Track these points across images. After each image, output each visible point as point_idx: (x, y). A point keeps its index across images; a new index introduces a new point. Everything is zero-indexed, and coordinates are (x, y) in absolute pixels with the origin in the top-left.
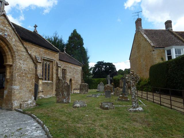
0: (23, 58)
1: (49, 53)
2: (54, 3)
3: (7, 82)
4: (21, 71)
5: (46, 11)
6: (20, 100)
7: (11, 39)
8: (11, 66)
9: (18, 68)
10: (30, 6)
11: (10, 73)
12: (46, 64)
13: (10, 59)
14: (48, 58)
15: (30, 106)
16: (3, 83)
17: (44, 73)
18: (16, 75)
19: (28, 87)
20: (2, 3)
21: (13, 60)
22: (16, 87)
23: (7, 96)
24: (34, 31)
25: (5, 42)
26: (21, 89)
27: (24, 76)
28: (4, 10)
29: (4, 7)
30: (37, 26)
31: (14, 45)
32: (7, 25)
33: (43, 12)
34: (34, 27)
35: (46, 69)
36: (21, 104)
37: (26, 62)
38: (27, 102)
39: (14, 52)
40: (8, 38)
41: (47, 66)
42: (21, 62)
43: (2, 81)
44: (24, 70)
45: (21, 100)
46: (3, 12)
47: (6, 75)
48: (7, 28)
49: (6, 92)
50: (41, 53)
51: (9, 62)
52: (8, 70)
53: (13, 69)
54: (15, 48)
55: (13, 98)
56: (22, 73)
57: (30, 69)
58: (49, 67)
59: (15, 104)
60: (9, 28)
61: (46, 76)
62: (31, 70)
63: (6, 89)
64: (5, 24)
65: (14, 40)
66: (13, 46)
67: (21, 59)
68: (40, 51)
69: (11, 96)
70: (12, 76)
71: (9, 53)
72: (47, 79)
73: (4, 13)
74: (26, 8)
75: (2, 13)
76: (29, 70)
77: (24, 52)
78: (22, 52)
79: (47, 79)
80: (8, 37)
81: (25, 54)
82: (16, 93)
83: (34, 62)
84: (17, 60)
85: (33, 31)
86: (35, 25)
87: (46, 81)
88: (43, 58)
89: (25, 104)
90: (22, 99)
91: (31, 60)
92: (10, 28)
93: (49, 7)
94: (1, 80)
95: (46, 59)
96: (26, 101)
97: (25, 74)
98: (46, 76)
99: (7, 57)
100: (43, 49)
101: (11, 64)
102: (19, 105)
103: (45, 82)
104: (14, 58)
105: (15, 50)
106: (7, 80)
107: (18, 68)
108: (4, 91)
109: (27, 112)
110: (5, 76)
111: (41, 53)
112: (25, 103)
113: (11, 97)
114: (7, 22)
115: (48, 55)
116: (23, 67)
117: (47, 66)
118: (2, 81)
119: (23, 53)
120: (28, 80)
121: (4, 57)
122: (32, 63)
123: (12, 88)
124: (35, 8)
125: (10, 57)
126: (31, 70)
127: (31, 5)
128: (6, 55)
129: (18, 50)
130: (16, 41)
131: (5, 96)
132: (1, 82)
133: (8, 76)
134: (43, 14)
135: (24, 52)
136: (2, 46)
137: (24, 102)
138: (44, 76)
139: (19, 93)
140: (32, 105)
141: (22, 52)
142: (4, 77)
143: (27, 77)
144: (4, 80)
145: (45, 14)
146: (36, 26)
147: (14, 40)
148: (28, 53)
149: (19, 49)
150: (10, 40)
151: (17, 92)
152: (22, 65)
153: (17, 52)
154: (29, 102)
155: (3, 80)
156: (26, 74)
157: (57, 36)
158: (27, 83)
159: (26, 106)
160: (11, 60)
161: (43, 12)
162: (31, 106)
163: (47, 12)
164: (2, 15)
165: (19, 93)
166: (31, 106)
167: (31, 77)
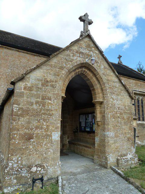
0: (116, 91)
1: (141, 84)
2: (134, 36)
3: (98, 126)
4: (115, 110)
5: (125, 47)
6: (117, 153)
7: (99, 66)
8: (101, 103)
9: (110, 105)
10: (110, 46)
11: (101, 113)
12: (138, 99)
13: (99, 94)
14: (140, 92)
15: (130, 162)
16: (92, 126)
17: (137, 111)
18: (109, 116)
19: (125, 133)
20: (86, 21)
21: (103, 95)
22: (110, 134)
23: (99, 145)
24: (119, 63)
25: (92, 72)
26: (116, 136)
27: (119, 117)
28: (89, 29)
29: (87, 27)
30: (121, 57)
31: (103, 74)
32: (93, 49)
33: (123, 48)
34: (118, 58)
35: (138, 106)
36: (118, 160)
37: (119, 97)
38: (126, 157)
39: (104, 84)
40: (95, 66)
41: (140, 102)
42: (114, 97)
43: (91, 123)
44: (119, 108)
45: (117, 153)
46: (87, 32)
47: (96, 116)
48: (93, 52)
49: (97, 140)
50: (132, 85)
51: (99, 98)
52: (98, 109)
53: (104, 108)
54: (104, 78)
55: (108, 150)
56: (116, 113)
57: (125, 106)
58: (142, 103)
59: (111, 159)
60: (96, 51)
61: (139, 114)
62: (127, 107)
63: (97, 136)
64: (91, 48)
65: (102, 69)
66: (102, 75)
67: (114, 93)
68: (130, 83)
69: (104, 146)
70: (103, 117)
71: (98, 86)
72: (141, 119)
73: (88, 33)
74: (106, 49)
75: (87, 34)
76: (125, 108)
77: (116, 82)
78: (114, 82)
79: (141, 119)
80: (96, 64)
81: (117, 86)
82: (110, 142)
83: (130, 96)
84: (108, 95)
85: (116, 62)
86: (119, 55)
87: (140, 122)
88: (134, 92)
89: (124, 159)
90: (118, 151)
91: (127, 94)
92: (97, 52)
93: (129, 41)
94: (91, 122)
95: (138, 92)
96: (125, 155)
97: (120, 114)
98: (139, 114)
99: (96, 91)
100: (134, 80)
101: (101, 100)
102: (115, 160)
103: (140, 124)
104: (105, 93)
105: (105, 81)
106: (97, 124)
107: (110, 105)
108: (94, 139)
109: (132, 180)
110: (94, 117)
111: (132, 85)
112: (124, 157)
113: (105, 148)
114: (92, 45)
115: (141, 87)
116: (118, 103)
117: (140, 102)
118: (91, 123)
119: (115, 84)
120: (125, 123)
121: (92, 92)
122: (128, 97)
123: (105, 135)
124: (115, 46)
125: (100, 91)
126: (127, 107)
127: (111, 45)
128: (94, 90)
129: (108, 80)
130: (105, 68)
131: (96, 145)
132: (91, 124)
133: (99, 117)
134: (123, 50)
135: (116, 82)
136: (89, 77)
137: (121, 156)
138: (137, 115)
139: (115, 143)
140: (133, 162)
141: (114, 82)
142: (94, 118)
143: (123, 117)
144: (93, 122)
145: (125, 50)
146: (120, 57)
147: (103, 67)
148: (122, 83)
149: (110, 78)
150: (98, 67)
151: (111, 142)
152: (115, 101)
153: (108, 83)
154: (129, 156)
155: (92, 122)
156: (121, 114)
157: (141, 66)
158: (123, 127)
159: (126, 163)
160: (101, 95)
161: (123, 48)
162: (132, 164)
163: (127, 47)
164: (86, 37)
165: (115, 143)
166: (132, 164)
167: (128, 119)
